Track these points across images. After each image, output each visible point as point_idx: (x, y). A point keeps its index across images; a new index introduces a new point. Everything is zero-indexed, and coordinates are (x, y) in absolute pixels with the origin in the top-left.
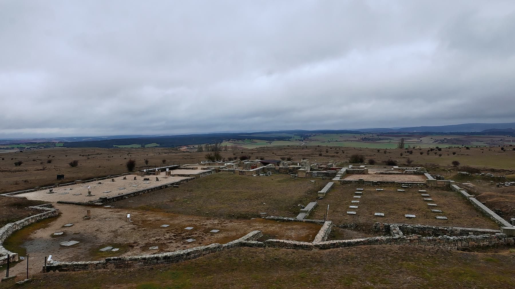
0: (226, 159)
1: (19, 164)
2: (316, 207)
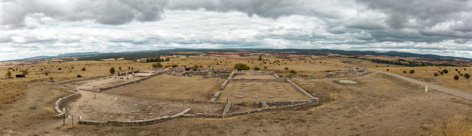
0: (164, 67)
1: (60, 69)
2: (220, 94)
